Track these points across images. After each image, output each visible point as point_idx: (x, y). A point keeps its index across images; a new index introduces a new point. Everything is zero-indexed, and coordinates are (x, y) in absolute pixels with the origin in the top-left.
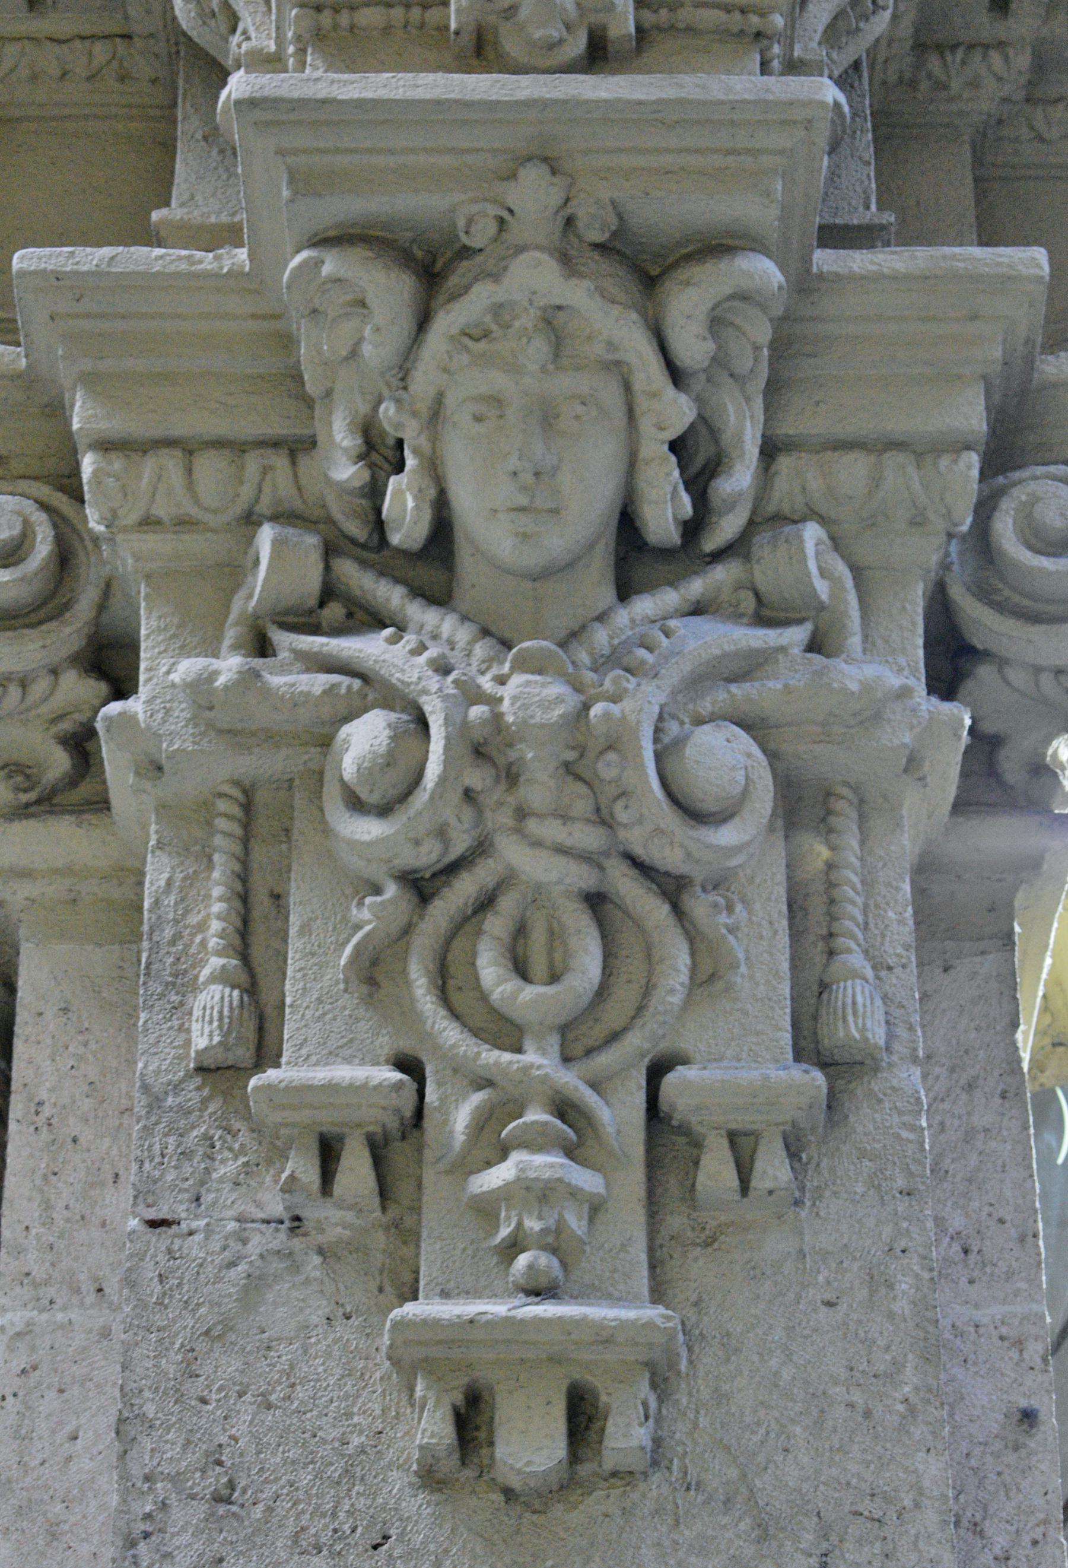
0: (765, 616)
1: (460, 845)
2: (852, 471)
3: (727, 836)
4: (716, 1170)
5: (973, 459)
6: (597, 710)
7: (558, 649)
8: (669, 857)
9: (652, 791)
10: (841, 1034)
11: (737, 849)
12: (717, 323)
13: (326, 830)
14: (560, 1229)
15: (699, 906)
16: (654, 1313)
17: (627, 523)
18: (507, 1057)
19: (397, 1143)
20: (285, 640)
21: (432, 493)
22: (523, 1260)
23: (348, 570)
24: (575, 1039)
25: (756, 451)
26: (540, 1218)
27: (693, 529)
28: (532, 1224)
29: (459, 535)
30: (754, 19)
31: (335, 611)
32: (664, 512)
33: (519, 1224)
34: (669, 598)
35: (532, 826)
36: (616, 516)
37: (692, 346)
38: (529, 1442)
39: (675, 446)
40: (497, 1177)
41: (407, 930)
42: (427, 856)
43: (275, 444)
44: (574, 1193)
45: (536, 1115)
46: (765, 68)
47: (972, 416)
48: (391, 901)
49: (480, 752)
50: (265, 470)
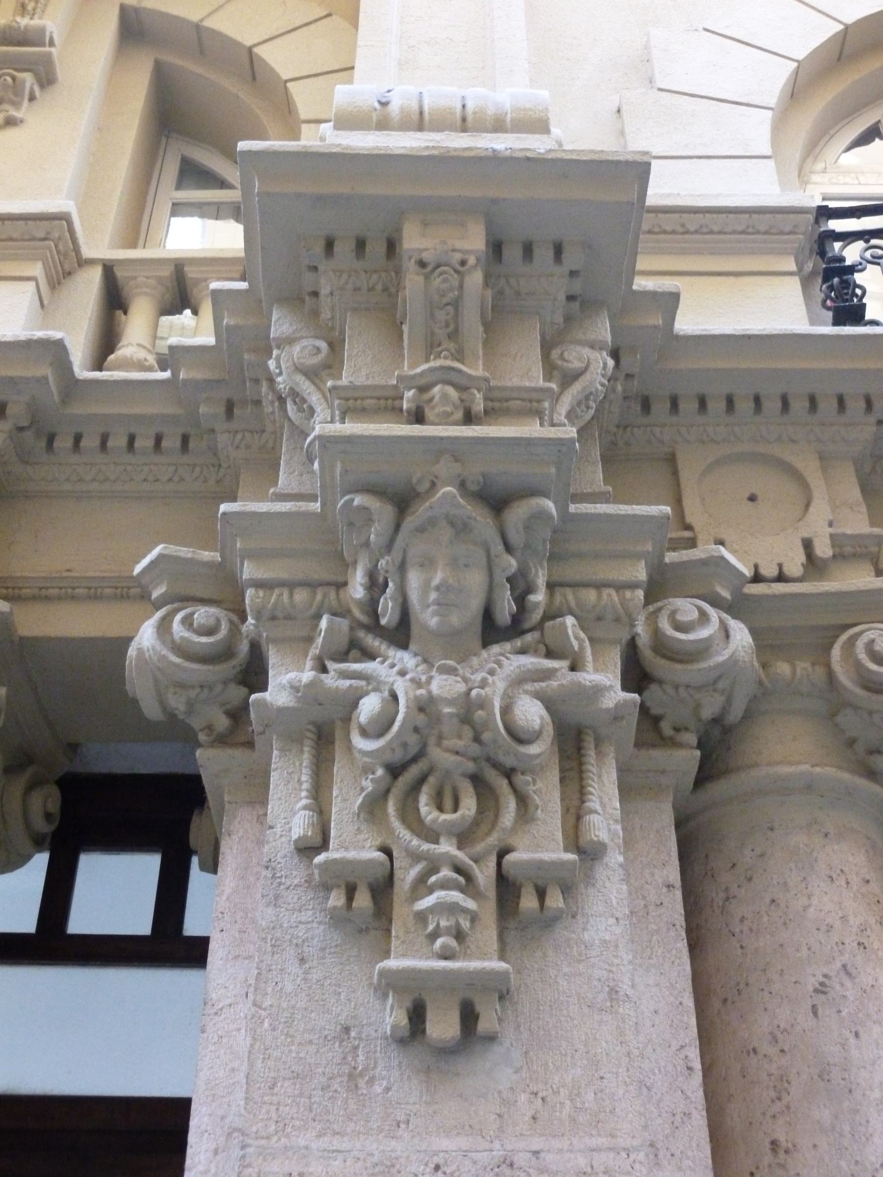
0: (550, 654)
1: (413, 751)
2: (591, 595)
3: (533, 749)
4: (528, 902)
5: (640, 594)
6: (474, 693)
7: (472, 863)
8: (509, 761)
9: (501, 733)
10: (589, 838)
11: (539, 755)
12: (528, 527)
13: (349, 746)
14: (458, 925)
15: (520, 779)
16: (503, 966)
17: (488, 615)
18: (433, 846)
19: (383, 888)
20: (331, 666)
21: (400, 600)
22: (439, 942)
23: (361, 634)
24: (463, 838)
25: (544, 588)
26: (448, 920)
27: (517, 619)
28: (444, 923)
29: (413, 621)
30: (535, 404)
31: (354, 653)
32: (505, 608)
33: (438, 924)
34: (507, 646)
35: (446, 743)
36: (481, 612)
37: (516, 537)
38: (443, 1026)
39: (509, 580)
40: (428, 901)
41: (388, 791)
42: (398, 756)
43: (328, 584)
44: (465, 910)
45: (446, 873)
46: (541, 425)
47: (641, 574)
48: (380, 778)
49: (421, 709)
50: (325, 596)
